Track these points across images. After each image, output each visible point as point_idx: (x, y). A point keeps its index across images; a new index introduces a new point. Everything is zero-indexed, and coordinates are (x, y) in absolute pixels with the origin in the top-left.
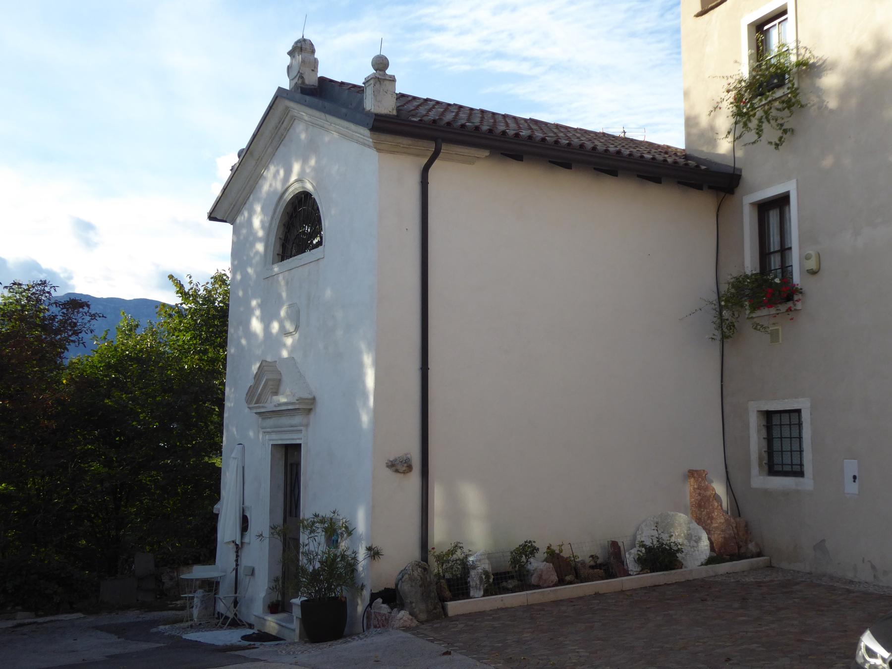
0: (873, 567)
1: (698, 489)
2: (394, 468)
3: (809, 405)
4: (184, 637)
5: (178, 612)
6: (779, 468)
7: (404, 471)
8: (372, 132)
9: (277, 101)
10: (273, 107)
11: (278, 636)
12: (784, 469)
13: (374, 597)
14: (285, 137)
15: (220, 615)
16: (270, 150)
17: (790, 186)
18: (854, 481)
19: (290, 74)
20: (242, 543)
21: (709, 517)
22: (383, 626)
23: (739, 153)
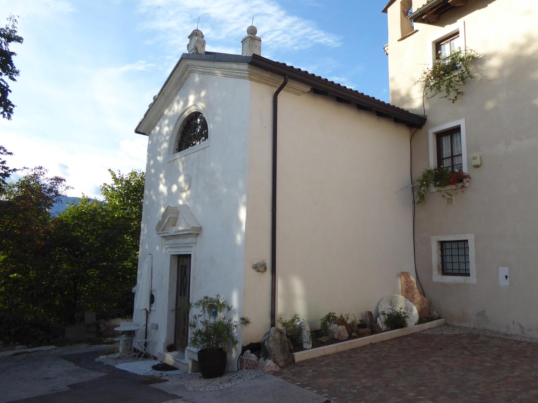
0: (521, 327)
1: (406, 282)
2: (257, 269)
3: (473, 237)
4: (116, 367)
5: (109, 346)
6: (449, 271)
7: (263, 271)
8: (250, 66)
9: (182, 61)
10: (179, 65)
11: (174, 366)
12: (454, 272)
13: (244, 349)
14: (184, 84)
15: (135, 350)
16: (174, 92)
17: (462, 123)
18: (506, 279)
19: (189, 49)
20: (150, 310)
21: (412, 298)
22: (253, 368)
23: (427, 107)
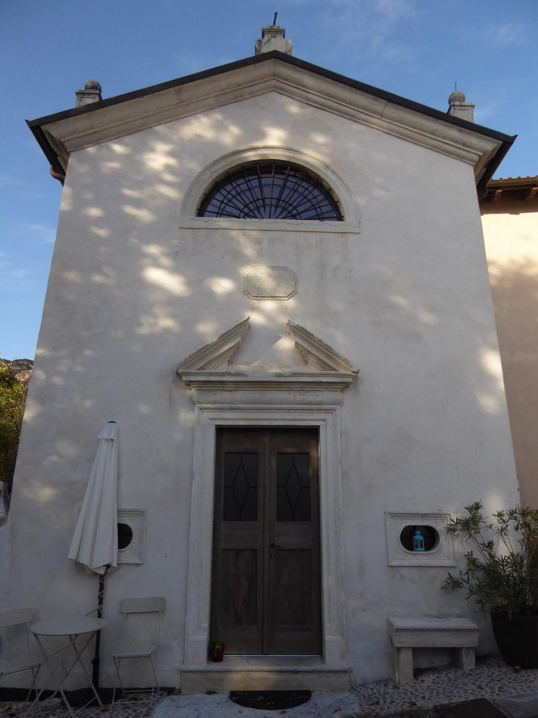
14: (243, 100)
